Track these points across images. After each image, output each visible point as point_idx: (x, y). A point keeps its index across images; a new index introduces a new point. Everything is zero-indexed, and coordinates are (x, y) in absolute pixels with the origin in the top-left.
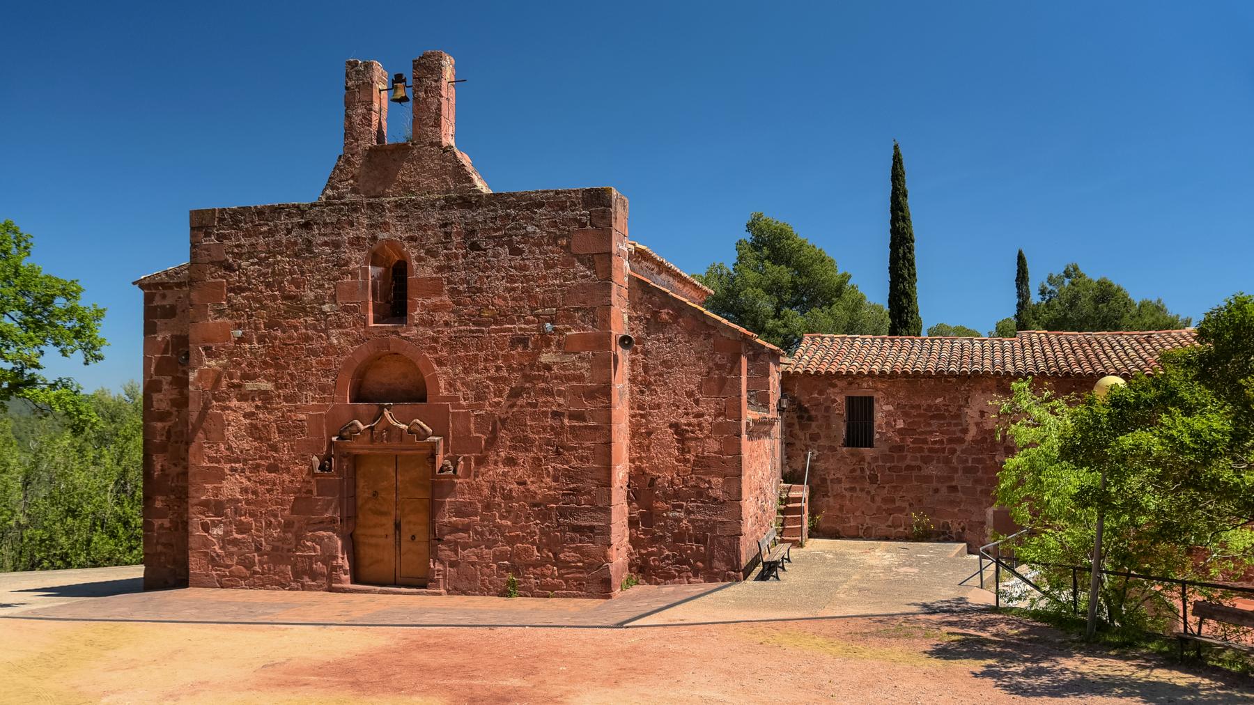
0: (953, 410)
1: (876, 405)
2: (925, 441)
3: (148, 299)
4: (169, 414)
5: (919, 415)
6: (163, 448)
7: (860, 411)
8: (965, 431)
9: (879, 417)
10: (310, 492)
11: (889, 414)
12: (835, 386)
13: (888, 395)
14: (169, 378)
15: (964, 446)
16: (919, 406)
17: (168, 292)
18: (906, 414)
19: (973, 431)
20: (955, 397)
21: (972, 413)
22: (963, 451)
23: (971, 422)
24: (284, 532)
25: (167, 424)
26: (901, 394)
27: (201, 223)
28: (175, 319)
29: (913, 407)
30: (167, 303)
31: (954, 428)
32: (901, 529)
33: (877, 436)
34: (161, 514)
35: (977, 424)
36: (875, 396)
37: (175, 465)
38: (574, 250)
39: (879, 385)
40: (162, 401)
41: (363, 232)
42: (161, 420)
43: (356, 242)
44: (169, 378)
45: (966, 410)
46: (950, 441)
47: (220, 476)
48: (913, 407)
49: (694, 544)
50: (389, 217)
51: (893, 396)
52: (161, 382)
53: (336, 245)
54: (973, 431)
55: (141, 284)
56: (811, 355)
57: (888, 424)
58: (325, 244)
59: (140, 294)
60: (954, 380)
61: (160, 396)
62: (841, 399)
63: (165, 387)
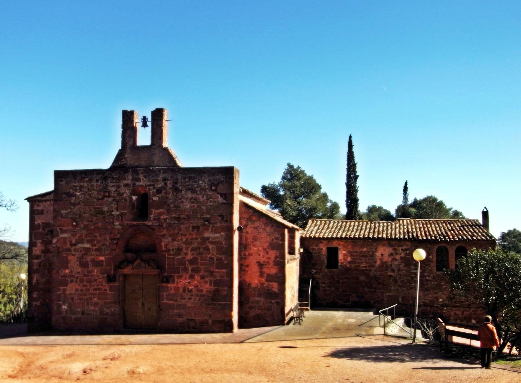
0: (371, 253)
1: (339, 252)
2: (359, 266)
3: (31, 207)
4: (40, 256)
5: (357, 256)
6: (37, 271)
7: (333, 253)
8: (375, 262)
9: (341, 256)
10: (106, 290)
11: (345, 255)
12: (322, 243)
13: (344, 246)
14: (40, 241)
15: (375, 268)
16: (357, 252)
17: (40, 204)
18: (352, 255)
19: (378, 262)
20: (372, 248)
21: (378, 254)
22: (375, 270)
23: (378, 259)
24: (95, 307)
25: (39, 261)
26: (350, 247)
27: (59, 175)
28: (43, 216)
29: (354, 252)
30: (40, 208)
31: (371, 261)
32: (350, 303)
33: (340, 264)
34: (36, 300)
35: (380, 259)
36: (339, 247)
37: (43, 278)
38: (218, 191)
39: (341, 243)
40: (37, 250)
41: (129, 182)
42: (36, 259)
43: (127, 185)
44: (40, 241)
45: (376, 253)
46: (370, 266)
47: (66, 284)
48: (354, 252)
49: (264, 311)
50: (141, 176)
51: (346, 247)
52: (36, 243)
53: (119, 187)
54: (378, 262)
55: (29, 199)
56: (314, 229)
57: (344, 259)
58: (113, 186)
59: (27, 204)
60: (371, 241)
61: (36, 248)
62: (324, 249)
63: (39, 245)
